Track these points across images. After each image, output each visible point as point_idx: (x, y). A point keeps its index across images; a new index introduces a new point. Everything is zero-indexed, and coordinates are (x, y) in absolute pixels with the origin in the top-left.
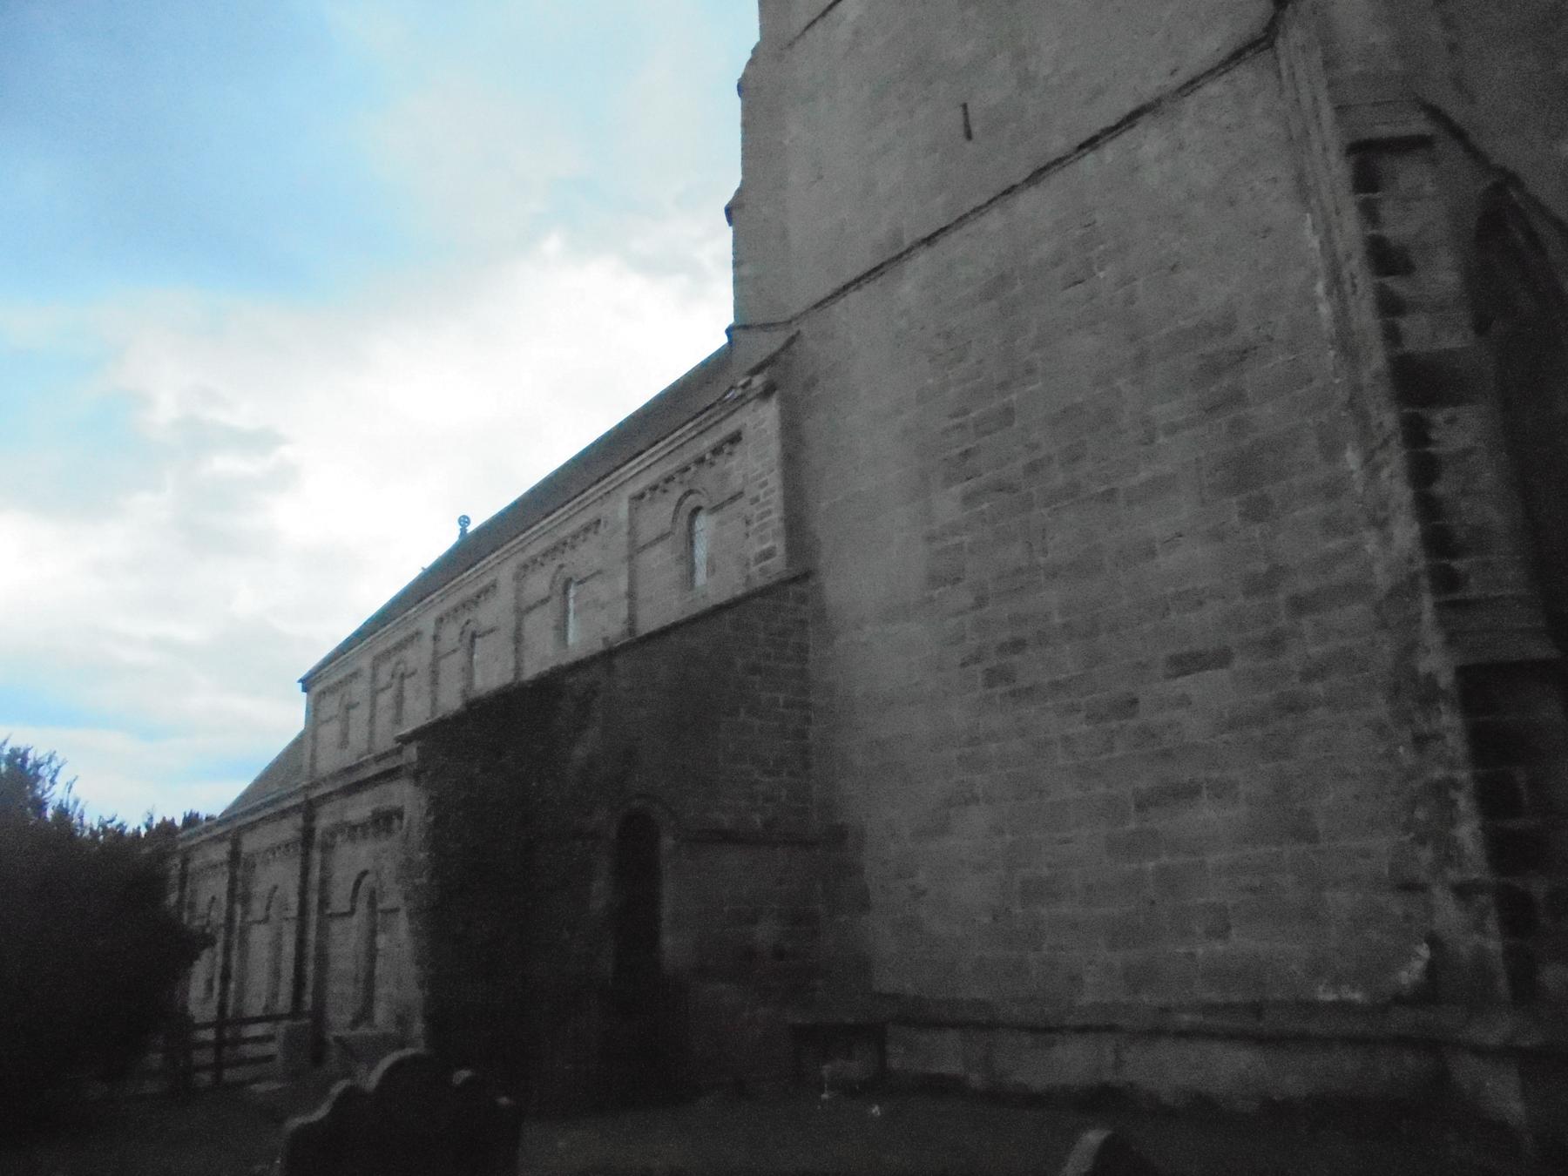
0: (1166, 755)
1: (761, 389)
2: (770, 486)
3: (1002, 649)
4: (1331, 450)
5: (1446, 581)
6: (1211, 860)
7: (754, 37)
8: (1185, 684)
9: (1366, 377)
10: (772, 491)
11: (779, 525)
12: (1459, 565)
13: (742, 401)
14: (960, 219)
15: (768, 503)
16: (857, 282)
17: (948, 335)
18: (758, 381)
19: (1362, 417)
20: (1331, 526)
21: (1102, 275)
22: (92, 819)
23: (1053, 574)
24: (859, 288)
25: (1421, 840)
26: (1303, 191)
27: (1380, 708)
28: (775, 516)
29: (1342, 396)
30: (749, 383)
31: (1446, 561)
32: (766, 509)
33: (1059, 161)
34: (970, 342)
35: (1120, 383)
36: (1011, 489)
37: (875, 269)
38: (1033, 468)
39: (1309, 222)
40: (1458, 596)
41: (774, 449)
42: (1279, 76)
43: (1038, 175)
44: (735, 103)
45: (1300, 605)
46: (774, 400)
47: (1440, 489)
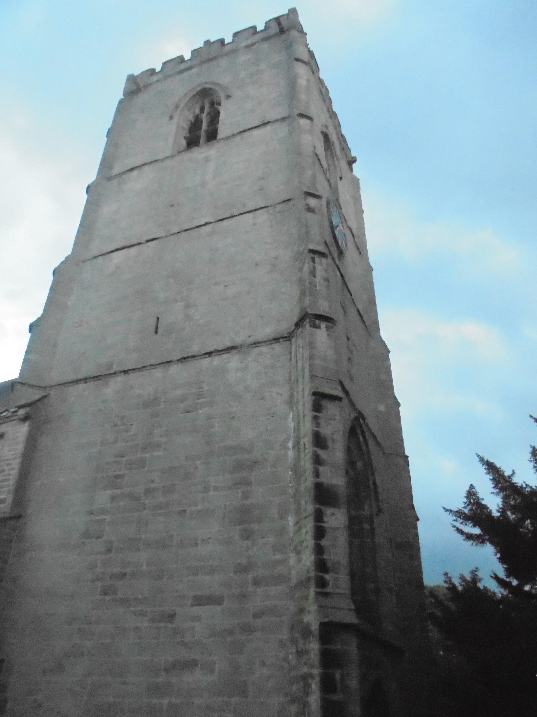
0: (184, 644)
1: (22, 417)
2: (13, 466)
3: (113, 576)
4: (282, 516)
5: (321, 583)
6: (197, 701)
7: (69, 252)
8: (196, 610)
9: (302, 488)
10: (13, 469)
11: (12, 488)
12: (327, 577)
13: (8, 419)
14: (144, 367)
15: (9, 475)
16: (85, 380)
17: (123, 418)
18: (22, 412)
19: (298, 503)
20: (276, 549)
21: (200, 411)
22: (493, 547)
23: (148, 545)
24: (86, 383)
25: (293, 701)
26: (291, 402)
27: (285, 635)
28: (11, 482)
29: (291, 491)
30: (16, 411)
31: (321, 574)
32: (6, 477)
33: (193, 356)
34: (132, 425)
35: (198, 462)
36: (137, 499)
37: (97, 377)
38: (148, 492)
39: (291, 416)
40: (325, 590)
41: (20, 448)
42: (291, 353)
43: (184, 359)
44: (50, 279)
45: (257, 582)
46: (27, 423)
47: (324, 542)
